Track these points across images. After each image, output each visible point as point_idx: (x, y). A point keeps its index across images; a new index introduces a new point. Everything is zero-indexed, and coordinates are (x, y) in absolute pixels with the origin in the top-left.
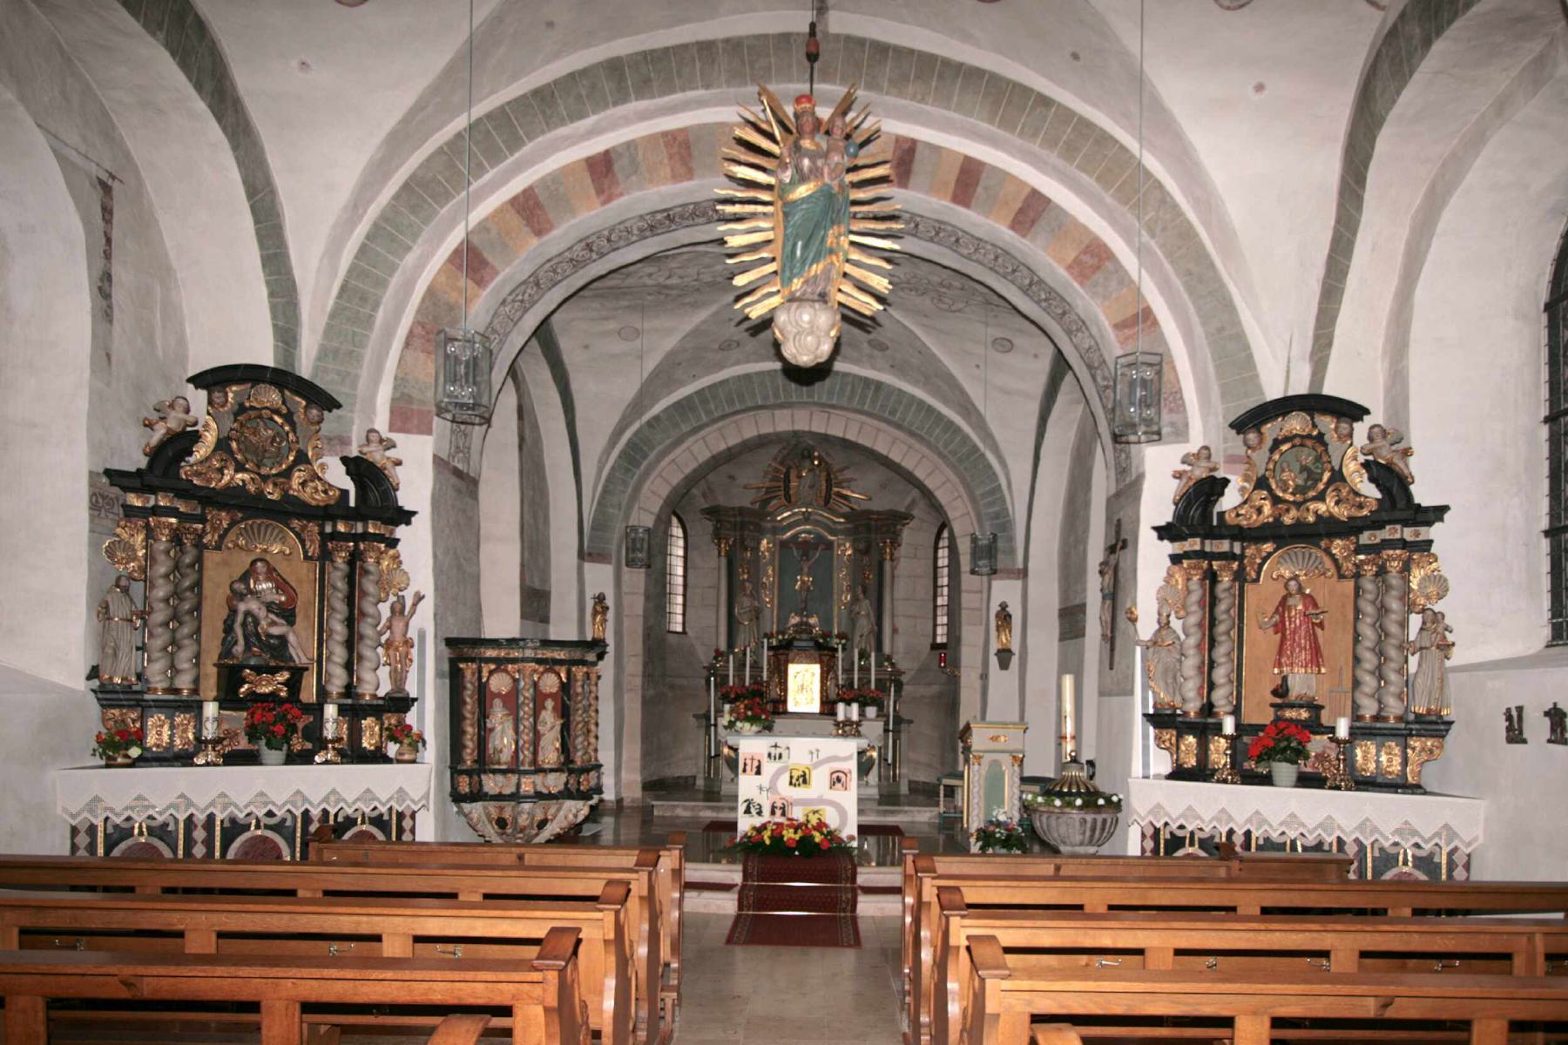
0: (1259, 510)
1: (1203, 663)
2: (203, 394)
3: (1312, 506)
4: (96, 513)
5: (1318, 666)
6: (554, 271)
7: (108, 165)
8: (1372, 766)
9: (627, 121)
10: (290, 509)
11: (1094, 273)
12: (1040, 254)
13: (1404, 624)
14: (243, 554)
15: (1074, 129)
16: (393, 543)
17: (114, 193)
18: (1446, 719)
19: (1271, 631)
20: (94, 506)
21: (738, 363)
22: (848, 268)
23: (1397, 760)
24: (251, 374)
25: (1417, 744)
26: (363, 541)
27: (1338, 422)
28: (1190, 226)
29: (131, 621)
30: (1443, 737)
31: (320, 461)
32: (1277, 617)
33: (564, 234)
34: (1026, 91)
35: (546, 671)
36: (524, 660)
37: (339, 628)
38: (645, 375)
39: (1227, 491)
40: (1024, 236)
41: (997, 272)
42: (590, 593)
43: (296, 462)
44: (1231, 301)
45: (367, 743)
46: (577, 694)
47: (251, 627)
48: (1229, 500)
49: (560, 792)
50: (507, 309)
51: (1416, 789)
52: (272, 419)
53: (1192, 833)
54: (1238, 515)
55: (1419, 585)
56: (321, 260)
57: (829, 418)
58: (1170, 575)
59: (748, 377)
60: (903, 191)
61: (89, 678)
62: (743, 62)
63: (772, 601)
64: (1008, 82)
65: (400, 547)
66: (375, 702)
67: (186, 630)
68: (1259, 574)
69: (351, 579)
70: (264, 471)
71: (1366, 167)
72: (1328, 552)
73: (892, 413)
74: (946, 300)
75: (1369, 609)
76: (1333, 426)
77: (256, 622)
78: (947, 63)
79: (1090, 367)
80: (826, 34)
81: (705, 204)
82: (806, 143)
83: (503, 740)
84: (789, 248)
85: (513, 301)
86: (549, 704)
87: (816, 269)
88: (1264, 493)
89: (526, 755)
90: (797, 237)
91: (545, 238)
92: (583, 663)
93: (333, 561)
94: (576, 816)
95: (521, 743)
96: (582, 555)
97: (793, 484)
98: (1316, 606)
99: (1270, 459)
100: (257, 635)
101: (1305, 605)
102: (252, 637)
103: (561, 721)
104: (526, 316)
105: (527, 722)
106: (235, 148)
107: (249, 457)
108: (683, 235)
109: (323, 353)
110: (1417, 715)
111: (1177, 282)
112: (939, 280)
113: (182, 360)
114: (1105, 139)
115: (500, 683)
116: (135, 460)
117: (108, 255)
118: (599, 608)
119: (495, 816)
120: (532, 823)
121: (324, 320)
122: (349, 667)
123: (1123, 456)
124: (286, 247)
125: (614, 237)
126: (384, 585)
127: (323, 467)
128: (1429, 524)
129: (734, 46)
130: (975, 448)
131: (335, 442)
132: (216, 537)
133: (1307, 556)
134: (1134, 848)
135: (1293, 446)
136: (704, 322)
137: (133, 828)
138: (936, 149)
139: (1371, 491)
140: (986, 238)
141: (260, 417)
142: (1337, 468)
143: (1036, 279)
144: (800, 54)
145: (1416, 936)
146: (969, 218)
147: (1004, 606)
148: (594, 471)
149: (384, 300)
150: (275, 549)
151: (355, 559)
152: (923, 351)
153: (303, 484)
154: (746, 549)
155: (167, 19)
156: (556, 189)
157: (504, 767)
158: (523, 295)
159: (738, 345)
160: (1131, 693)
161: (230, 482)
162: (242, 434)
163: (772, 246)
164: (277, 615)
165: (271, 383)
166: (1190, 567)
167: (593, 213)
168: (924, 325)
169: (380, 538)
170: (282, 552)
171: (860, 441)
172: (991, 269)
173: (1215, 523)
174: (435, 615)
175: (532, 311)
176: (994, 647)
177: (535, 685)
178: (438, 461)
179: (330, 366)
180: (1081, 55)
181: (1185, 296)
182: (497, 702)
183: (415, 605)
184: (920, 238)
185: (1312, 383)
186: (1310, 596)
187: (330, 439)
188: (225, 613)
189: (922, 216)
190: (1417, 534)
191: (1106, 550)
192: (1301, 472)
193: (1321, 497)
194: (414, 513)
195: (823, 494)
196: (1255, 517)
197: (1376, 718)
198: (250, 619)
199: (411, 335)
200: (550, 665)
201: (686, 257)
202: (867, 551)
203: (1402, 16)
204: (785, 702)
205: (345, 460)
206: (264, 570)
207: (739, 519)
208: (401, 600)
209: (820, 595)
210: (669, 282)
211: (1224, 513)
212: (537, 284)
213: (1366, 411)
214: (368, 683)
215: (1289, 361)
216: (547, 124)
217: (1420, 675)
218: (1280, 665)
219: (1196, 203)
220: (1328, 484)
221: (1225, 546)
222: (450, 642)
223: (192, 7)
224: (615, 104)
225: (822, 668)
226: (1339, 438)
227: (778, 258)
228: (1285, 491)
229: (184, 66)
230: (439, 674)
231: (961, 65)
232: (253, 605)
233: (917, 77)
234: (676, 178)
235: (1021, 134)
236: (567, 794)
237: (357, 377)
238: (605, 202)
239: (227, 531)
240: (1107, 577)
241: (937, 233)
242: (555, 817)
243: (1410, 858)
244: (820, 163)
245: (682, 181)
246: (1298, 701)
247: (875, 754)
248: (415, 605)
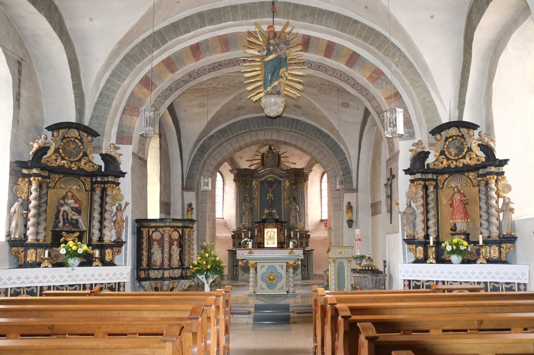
0: (442, 163)
3: (461, 161)
4: (12, 176)
5: (467, 219)
6: (177, 85)
7: (21, 56)
9: (205, 33)
10: (81, 173)
11: (377, 80)
13: (497, 202)
14: (62, 190)
15: (367, 31)
16: (118, 184)
21: (243, 115)
22: (288, 82)
24: (68, 125)
25: (504, 246)
30: (513, 243)
31: (91, 155)
37: (96, 215)
38: (208, 120)
39: (429, 156)
40: (351, 68)
41: (342, 80)
42: (186, 203)
43: (83, 156)
44: (428, 89)
46: (186, 239)
47: (65, 217)
48: (431, 160)
50: (160, 99)
52: (74, 141)
53: (423, 284)
54: (434, 165)
57: (279, 134)
58: (410, 187)
63: (257, 204)
64: (343, 16)
65: (120, 186)
66: (111, 243)
68: (443, 186)
70: (71, 160)
76: (467, 132)
77: (67, 215)
78: (321, 10)
79: (378, 113)
81: (233, 60)
83: (157, 257)
85: (162, 96)
87: (276, 83)
89: (166, 262)
97: (265, 159)
98: (465, 197)
99: (445, 144)
101: (461, 197)
103: (180, 249)
105: (166, 250)
106: (65, 48)
107: (66, 155)
109: (93, 117)
111: (407, 83)
113: (42, 121)
115: (156, 236)
117: (19, 86)
118: (190, 209)
122: (101, 230)
123: (391, 145)
124: (81, 81)
125: (199, 73)
126: (114, 198)
127: (93, 157)
128: (503, 166)
132: (53, 184)
135: (453, 140)
137: (21, 291)
138: (318, 39)
139: (482, 155)
140: (337, 68)
141: (71, 140)
142: (469, 147)
143: (356, 82)
145: (497, 307)
147: (349, 203)
150: (75, 187)
153: (85, 164)
155: (45, 7)
156: (179, 57)
157: (158, 267)
158: (166, 94)
161: (59, 164)
163: (261, 76)
164: (75, 212)
165: (75, 128)
166: (417, 184)
169: (113, 183)
170: (77, 189)
172: (339, 79)
177: (170, 236)
179: (95, 121)
181: (411, 88)
182: (155, 243)
183: (125, 207)
184: (312, 69)
185: (459, 117)
186: (463, 193)
188: (56, 211)
189: (313, 62)
190: (499, 170)
193: (464, 157)
194: (126, 173)
196: (441, 165)
198: (65, 213)
199: (125, 109)
204: (263, 243)
205: (101, 155)
206: (71, 195)
208: (120, 205)
210: (218, 86)
211: (429, 164)
212: (171, 90)
213: (479, 127)
215: (450, 109)
216: (176, 35)
220: (467, 152)
222: (137, 221)
223: (53, 3)
224: (201, 27)
228: (451, 155)
229: (50, 22)
230: (133, 233)
231: (326, 11)
232: (66, 208)
233: (310, 15)
234: (223, 51)
236: (182, 277)
237: (105, 125)
238: (196, 61)
239: (57, 182)
241: (319, 67)
242: (177, 286)
243: (504, 288)
245: (225, 52)
247: (300, 263)
248: (125, 207)
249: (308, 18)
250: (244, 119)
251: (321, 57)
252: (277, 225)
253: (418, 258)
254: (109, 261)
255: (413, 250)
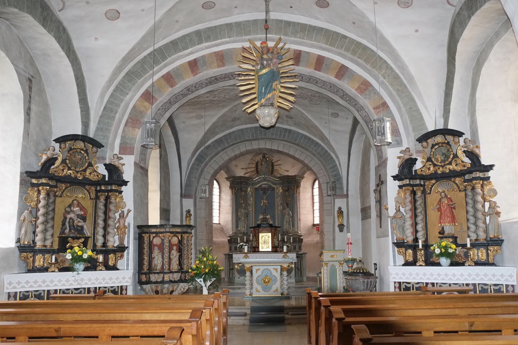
0: (429, 169)
1: (413, 223)
2: (58, 144)
3: (448, 167)
4: (22, 186)
5: (454, 223)
6: (176, 98)
8: (476, 258)
11: (365, 91)
12: (345, 85)
13: (483, 206)
16: (121, 192)
17: (33, 82)
18: (501, 239)
19: (437, 210)
20: (21, 184)
21: (238, 125)
23: (485, 255)
24: (74, 138)
25: (492, 249)
26: (111, 192)
27: (454, 138)
28: (398, 75)
29: (32, 222)
30: (501, 245)
31: (96, 165)
32: (438, 206)
33: (180, 86)
34: (338, 34)
35: (174, 236)
36: (166, 232)
37: (101, 222)
40: (340, 80)
43: (88, 166)
45: (111, 263)
47: (71, 223)
48: (418, 166)
49: (178, 280)
50: (160, 112)
51: (493, 264)
52: (80, 152)
53: (413, 286)
54: (422, 171)
55: (487, 192)
56: (98, 99)
58: (399, 193)
59: (242, 130)
60: (298, 67)
61: (17, 243)
62: (242, 29)
63: (252, 210)
64: (332, 31)
65: (123, 194)
66: (114, 249)
67: (49, 225)
68: (431, 191)
69: (106, 206)
70: (77, 170)
71: (455, 55)
72: (454, 182)
73: (295, 140)
74: (314, 101)
75: (470, 201)
76: (452, 139)
79: (366, 122)
80: (269, 19)
82: (265, 56)
83: (158, 261)
84: (260, 90)
85: (162, 109)
86: (175, 248)
87: (269, 96)
88: (430, 163)
89: (166, 266)
90: (263, 86)
91: (174, 88)
92: (187, 233)
93: (99, 199)
94: (184, 289)
95: (164, 262)
96: (182, 196)
97: (259, 167)
98: (452, 201)
99: (431, 151)
100: (74, 226)
101: (448, 201)
102: (72, 226)
103: (179, 254)
104: (166, 113)
105: (166, 255)
106: (72, 66)
108: (221, 84)
109: (97, 129)
110: (491, 238)
111: (394, 93)
112: (311, 94)
113: (50, 133)
114: (366, 48)
115: (157, 241)
116: (36, 167)
118: (188, 215)
119: (155, 289)
120: (168, 292)
121: (98, 118)
122: (104, 236)
126: (117, 207)
127: (97, 167)
128: (488, 171)
129: (238, 24)
130: (327, 152)
131: (101, 159)
132: (60, 193)
133: (447, 184)
134: (392, 289)
135: (439, 147)
136: (227, 112)
138: (308, 53)
139: (467, 160)
141: (77, 152)
142: (455, 153)
143: (345, 93)
144: (262, 26)
146: (320, 75)
147: (340, 209)
148: (186, 165)
149: (119, 111)
150: (80, 196)
151: (107, 198)
152: (306, 118)
153: (90, 173)
154: (242, 191)
157: (158, 271)
158: (165, 107)
159: (239, 119)
160: (388, 236)
161: (66, 174)
162: (70, 157)
164: (80, 219)
166: (405, 190)
167: (191, 79)
168: (305, 109)
169: (116, 191)
171: (284, 151)
172: (329, 91)
173: (414, 174)
174: (134, 217)
175: (168, 111)
176: (337, 224)
177: (170, 241)
178: (136, 164)
180: (356, 23)
182: (156, 248)
183: (128, 214)
184: (304, 82)
187: (99, 158)
188: (62, 218)
189: (304, 75)
190: (485, 175)
191: (376, 185)
192: (443, 155)
193: (450, 163)
194: (128, 182)
195: (271, 170)
196: (428, 171)
197: (477, 240)
198: (71, 221)
199: (127, 121)
200: (175, 234)
201: (220, 90)
202: (288, 190)
203: (461, 8)
204: (258, 247)
206: (77, 203)
207: (239, 181)
208: (123, 212)
209: (269, 208)
210: (214, 99)
211: (417, 170)
212: (170, 103)
213: (464, 134)
214: (111, 242)
215: (436, 118)
216: (175, 52)
217: (490, 224)
218: (441, 223)
219: (399, 67)
221: (418, 182)
222: (139, 227)
224: (198, 44)
225: (272, 234)
226: (455, 143)
227: (257, 93)
228: (437, 162)
230: (135, 239)
232: (72, 215)
233: (301, 31)
234: (219, 66)
235: (337, 48)
236: (181, 281)
237: (109, 137)
238: (194, 76)
239: (64, 190)
240: (377, 194)
241: (310, 80)
242: (176, 290)
243: (492, 290)
244: (269, 62)
246: (448, 236)
247: (293, 266)
248: (128, 214)
249: (298, 34)
250: (239, 130)
251: (311, 70)
252: (271, 229)
253: (407, 260)
254: (112, 265)
255: (403, 253)
